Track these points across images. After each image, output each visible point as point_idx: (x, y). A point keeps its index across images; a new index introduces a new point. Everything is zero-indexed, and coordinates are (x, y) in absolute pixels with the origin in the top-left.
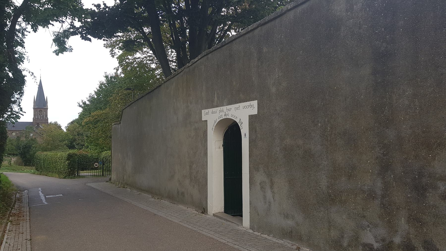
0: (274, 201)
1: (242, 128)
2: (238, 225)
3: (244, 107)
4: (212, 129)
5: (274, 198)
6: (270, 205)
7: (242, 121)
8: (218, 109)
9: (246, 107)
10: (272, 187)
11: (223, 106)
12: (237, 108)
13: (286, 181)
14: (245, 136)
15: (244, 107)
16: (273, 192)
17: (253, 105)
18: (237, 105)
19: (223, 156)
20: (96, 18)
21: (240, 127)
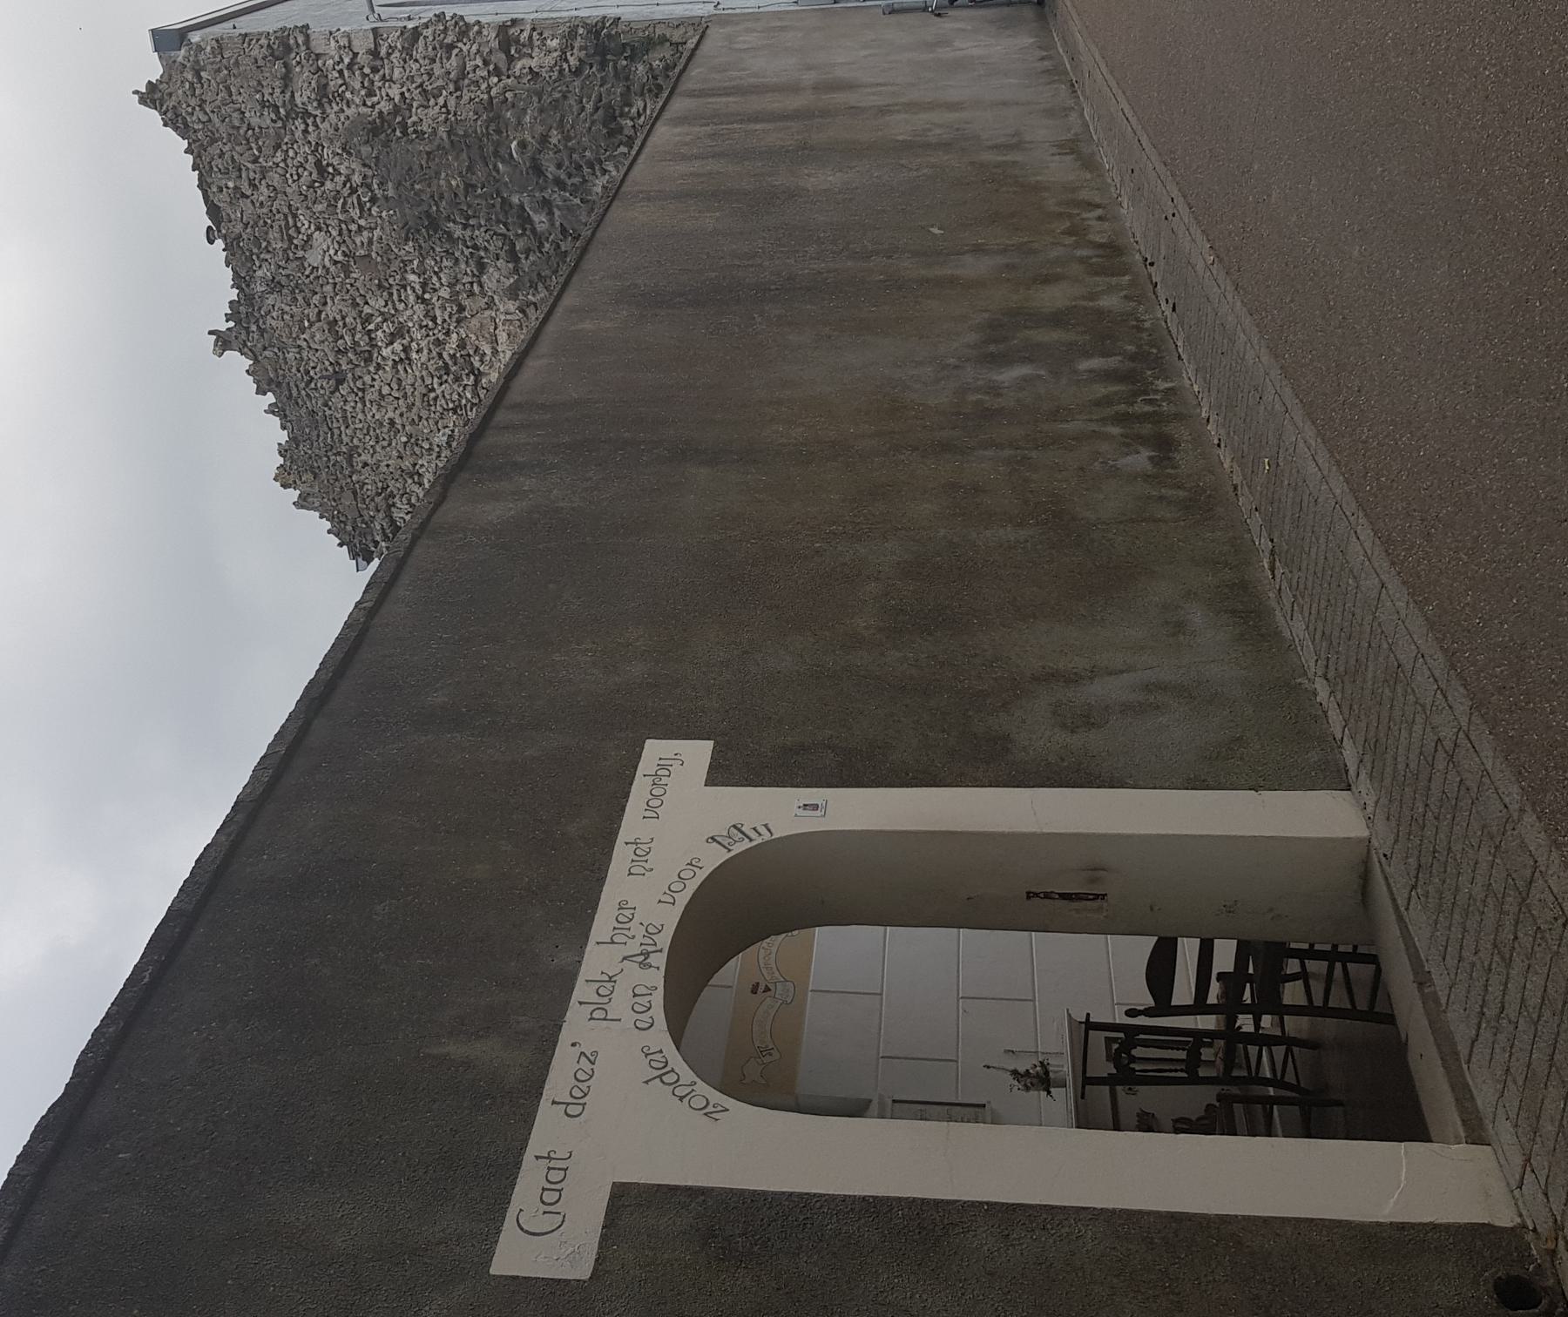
0: (1129, 669)
1: (763, 830)
2: (1379, 858)
3: (648, 814)
4: (708, 1112)
5: (1122, 672)
6: (1162, 687)
7: (720, 830)
8: (576, 1023)
9: (581, 1076)
10: (1073, 679)
11: (573, 976)
12: (641, 852)
13: (1027, 628)
14: (815, 807)
15: (652, 812)
16: (1094, 673)
17: (662, 762)
18: (621, 855)
19: (1004, 828)
20: (1251, 971)
21: (759, 841)
